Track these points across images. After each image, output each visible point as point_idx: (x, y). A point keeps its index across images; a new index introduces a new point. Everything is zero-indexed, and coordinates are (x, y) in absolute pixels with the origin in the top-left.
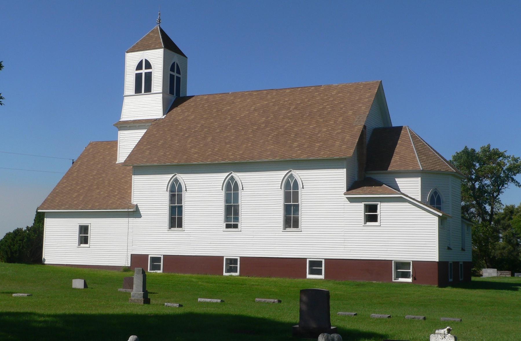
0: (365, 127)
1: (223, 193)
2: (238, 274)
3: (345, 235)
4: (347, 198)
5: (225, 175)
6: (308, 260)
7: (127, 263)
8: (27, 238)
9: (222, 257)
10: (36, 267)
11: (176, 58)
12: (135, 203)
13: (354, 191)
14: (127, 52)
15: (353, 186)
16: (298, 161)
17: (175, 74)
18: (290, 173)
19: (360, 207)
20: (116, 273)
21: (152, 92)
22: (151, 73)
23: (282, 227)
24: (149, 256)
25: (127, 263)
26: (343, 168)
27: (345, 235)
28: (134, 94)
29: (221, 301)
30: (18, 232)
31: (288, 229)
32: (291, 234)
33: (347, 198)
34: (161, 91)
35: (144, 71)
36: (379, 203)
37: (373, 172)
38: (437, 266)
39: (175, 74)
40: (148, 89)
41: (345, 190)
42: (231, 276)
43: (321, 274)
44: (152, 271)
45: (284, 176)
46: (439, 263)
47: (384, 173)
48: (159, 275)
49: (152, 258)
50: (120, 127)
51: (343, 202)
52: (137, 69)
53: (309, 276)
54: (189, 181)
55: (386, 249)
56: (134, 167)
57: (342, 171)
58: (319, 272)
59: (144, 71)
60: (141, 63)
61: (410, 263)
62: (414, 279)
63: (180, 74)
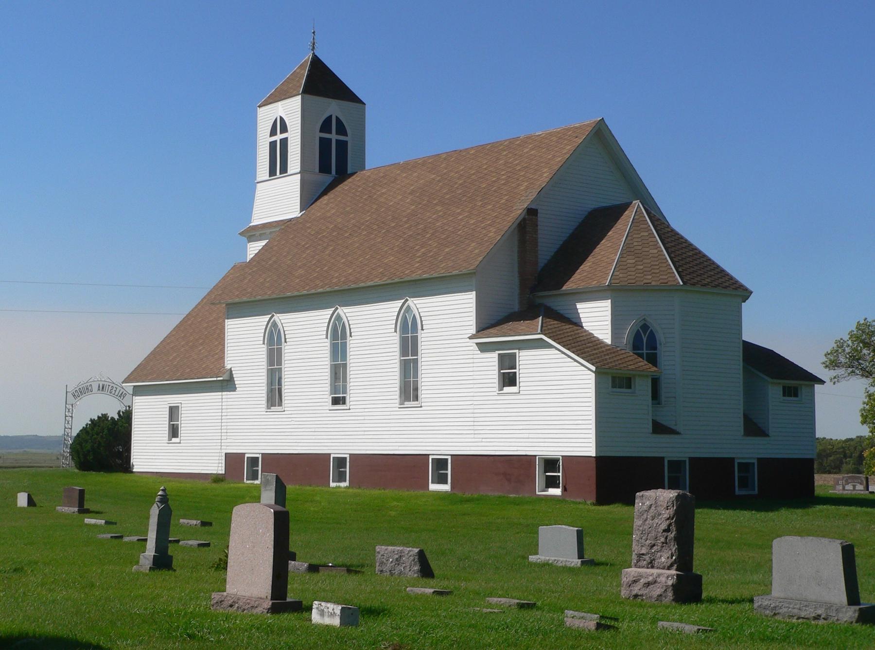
0: (532, 212)
1: (327, 343)
2: (346, 484)
3: (476, 411)
4: (477, 344)
5: (398, 303)
6: (431, 457)
7: (217, 467)
8: (109, 430)
9: (663, 459)
10: (118, 478)
11: (334, 108)
12: (228, 367)
13: (492, 331)
14: (259, 107)
15: (488, 322)
16: (415, 281)
17: (334, 136)
18: (406, 305)
19: (492, 358)
20: (200, 484)
21: (289, 172)
22: (286, 139)
23: (265, 406)
24: (332, 456)
25: (217, 467)
26: (472, 291)
27: (476, 411)
28: (267, 178)
29: (106, 523)
30: (104, 417)
31: (407, 404)
32: (410, 413)
33: (477, 344)
34: (299, 170)
35: (278, 137)
36: (517, 351)
37: (551, 293)
38: (593, 465)
39: (334, 136)
40: (284, 170)
41: (473, 330)
42: (339, 487)
43: (446, 483)
44: (249, 482)
45: (329, 316)
46: (600, 460)
47: (550, 296)
48: (553, 498)
49: (670, 462)
50: (261, 235)
51: (472, 352)
52: (271, 135)
53: (433, 487)
54: (356, 316)
55: (526, 436)
56: (227, 305)
57: (470, 296)
58: (445, 482)
59: (278, 137)
60: (329, 118)
61: (558, 460)
62: (565, 489)
63: (345, 134)
